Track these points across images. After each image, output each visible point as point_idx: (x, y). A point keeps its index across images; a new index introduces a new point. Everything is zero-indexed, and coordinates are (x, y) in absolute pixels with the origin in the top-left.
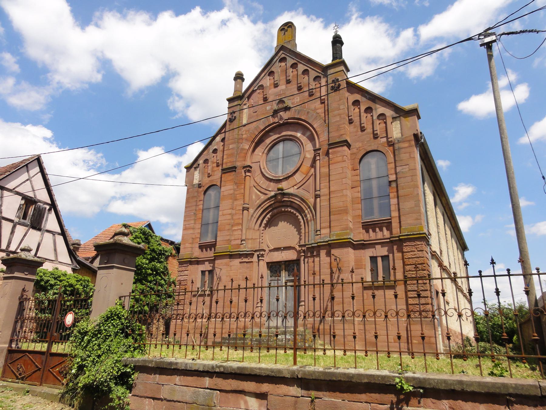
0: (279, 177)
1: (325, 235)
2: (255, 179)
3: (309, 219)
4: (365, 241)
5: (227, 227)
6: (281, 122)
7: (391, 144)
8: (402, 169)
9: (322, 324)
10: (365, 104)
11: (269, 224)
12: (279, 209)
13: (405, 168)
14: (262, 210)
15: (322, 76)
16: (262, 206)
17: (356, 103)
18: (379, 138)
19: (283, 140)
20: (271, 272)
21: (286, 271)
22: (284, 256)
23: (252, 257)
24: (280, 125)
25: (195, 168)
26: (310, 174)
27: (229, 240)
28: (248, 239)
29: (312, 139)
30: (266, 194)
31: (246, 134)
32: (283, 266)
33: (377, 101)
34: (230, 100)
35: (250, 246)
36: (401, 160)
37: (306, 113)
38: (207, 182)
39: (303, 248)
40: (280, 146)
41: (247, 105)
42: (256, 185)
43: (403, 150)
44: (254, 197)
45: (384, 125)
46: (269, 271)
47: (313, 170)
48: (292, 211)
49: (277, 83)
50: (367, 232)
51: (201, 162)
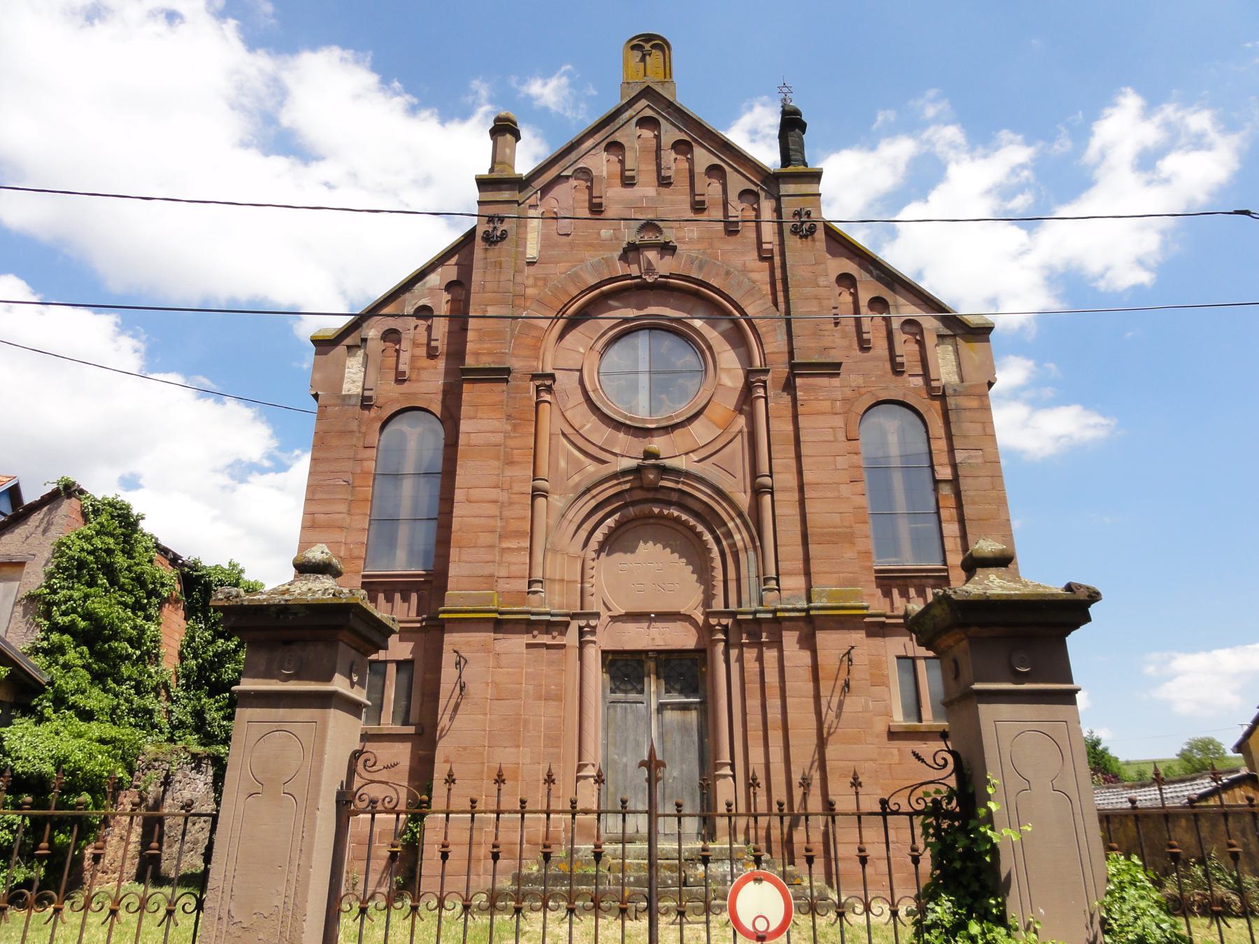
0: (644, 421)
1: (790, 593)
2: (568, 414)
3: (740, 544)
4: (501, 613)
5: (485, 538)
6: (650, 280)
7: (939, 395)
8: (970, 457)
9: (802, 828)
10: (868, 289)
11: (610, 544)
12: (645, 508)
13: (976, 457)
14: (593, 503)
15: (762, 194)
16: (594, 492)
17: (846, 280)
18: (906, 375)
19: (651, 328)
20: (613, 678)
21: (658, 678)
22: (657, 637)
23: (563, 633)
24: (643, 287)
25: (349, 347)
26: (735, 429)
27: (492, 576)
28: (553, 581)
29: (737, 338)
30: (603, 462)
31: (535, 286)
32: (651, 665)
33: (897, 286)
34: (482, 183)
35: (557, 600)
36: (965, 437)
37: (723, 272)
38: (390, 394)
39: (724, 621)
40: (642, 342)
41: (540, 210)
42: (568, 430)
43: (968, 413)
44: (563, 464)
45: (916, 347)
46: (607, 677)
47: (741, 421)
48: (684, 517)
49: (633, 178)
50: (887, 594)
51: (372, 331)
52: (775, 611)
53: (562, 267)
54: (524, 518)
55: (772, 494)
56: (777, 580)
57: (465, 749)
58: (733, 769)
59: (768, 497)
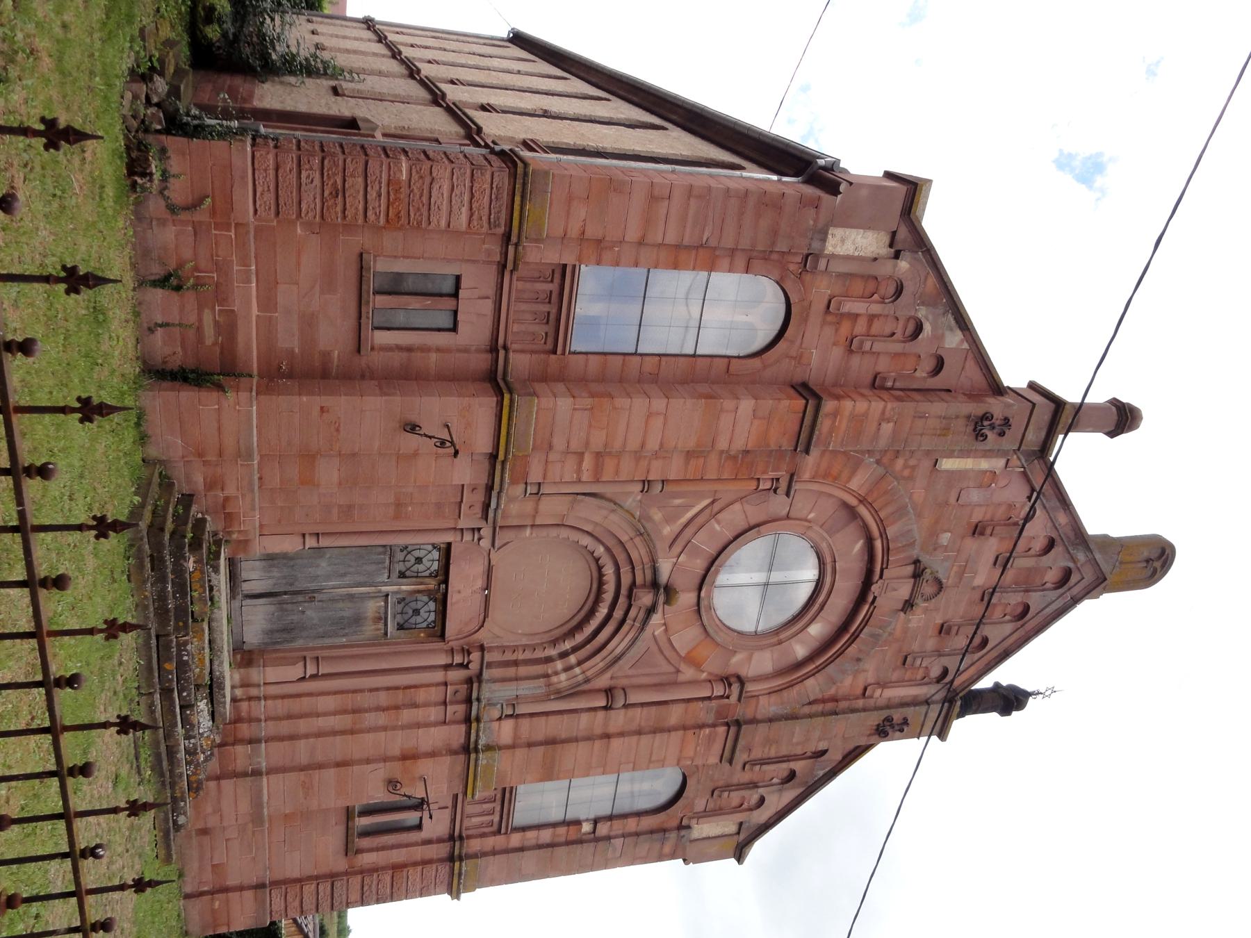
2: (737, 506)
4: (503, 463)
31: (905, 466)
42: (717, 507)
52: (478, 720)
53: (919, 494)
54: (617, 473)
55: (606, 708)
56: (511, 716)
57: (338, 430)
58: (314, 677)
59: (603, 703)
